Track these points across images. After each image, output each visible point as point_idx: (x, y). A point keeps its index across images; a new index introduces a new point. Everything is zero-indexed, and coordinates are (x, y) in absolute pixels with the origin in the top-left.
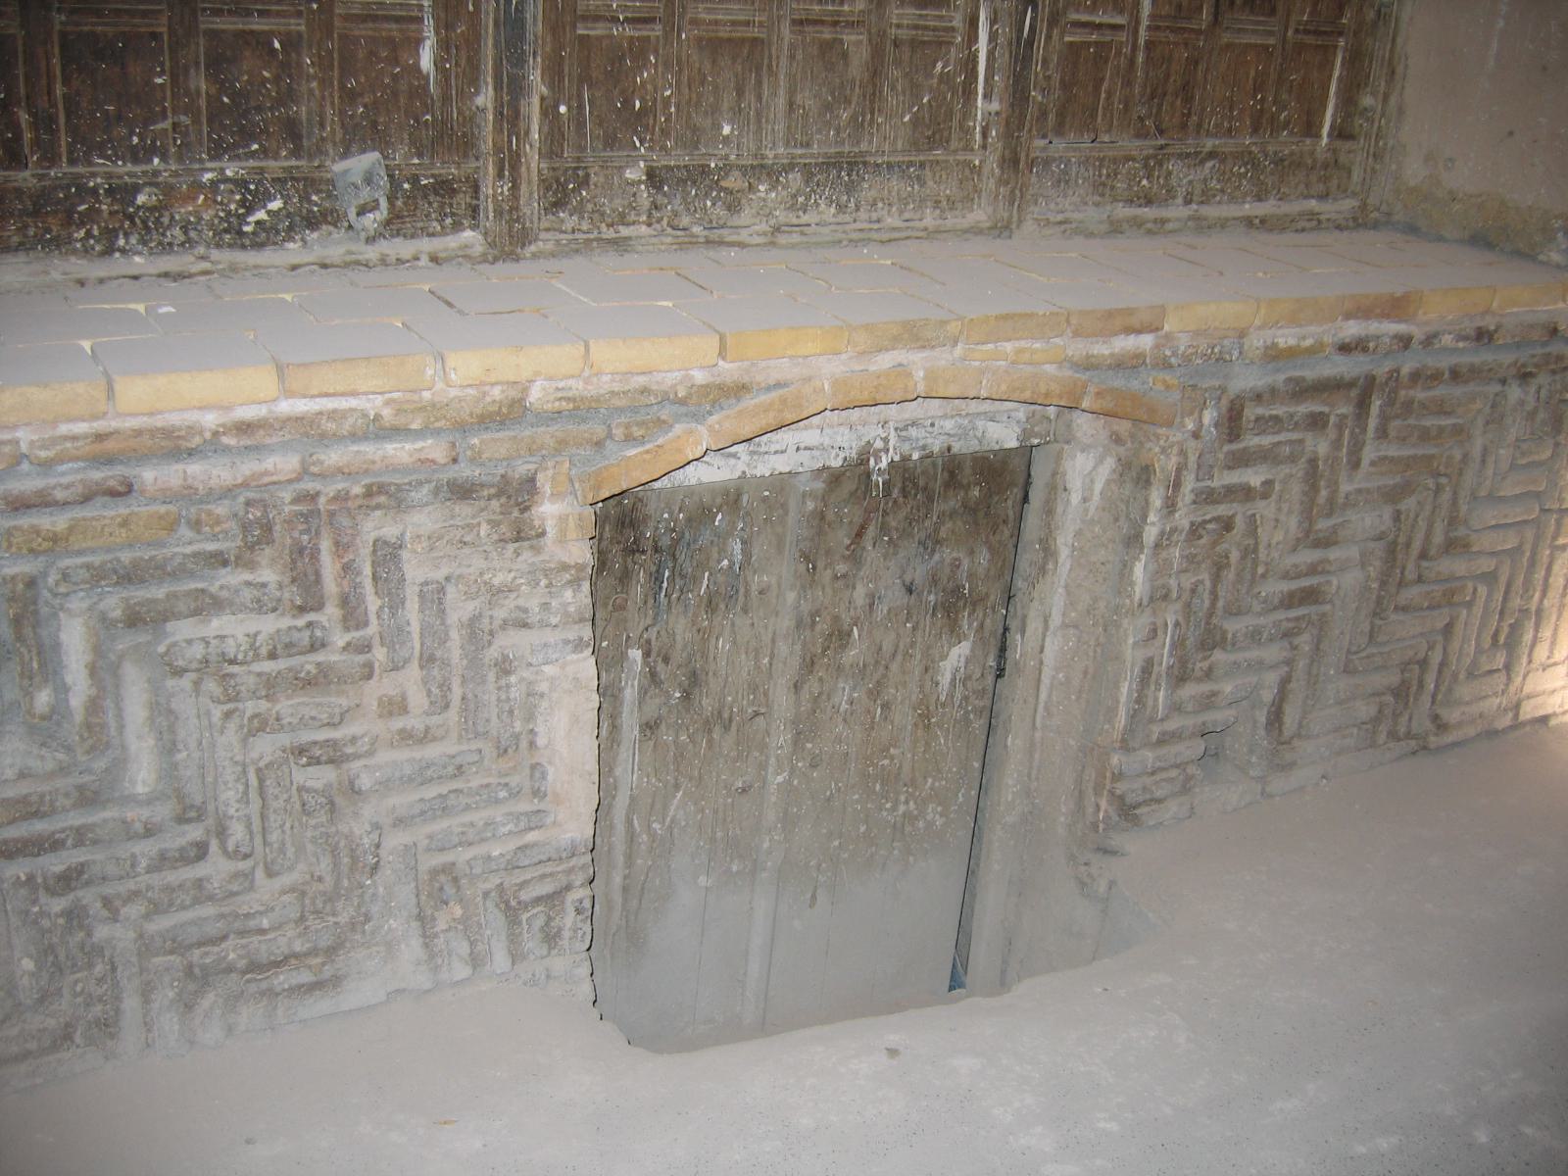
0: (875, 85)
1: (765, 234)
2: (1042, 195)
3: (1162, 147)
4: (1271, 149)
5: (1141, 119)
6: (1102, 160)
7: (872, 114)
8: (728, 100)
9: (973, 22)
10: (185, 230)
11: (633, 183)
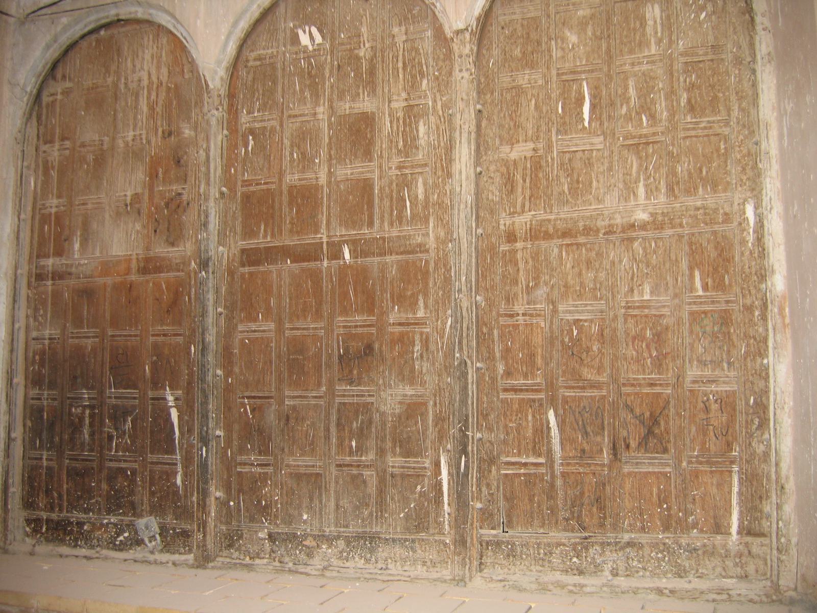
0: (382, 498)
1: (318, 570)
2: (497, 563)
3: (586, 538)
4: (683, 542)
5: (567, 520)
6: (539, 544)
7: (381, 512)
8: (306, 501)
9: (437, 464)
10: (98, 540)
11: (262, 539)
